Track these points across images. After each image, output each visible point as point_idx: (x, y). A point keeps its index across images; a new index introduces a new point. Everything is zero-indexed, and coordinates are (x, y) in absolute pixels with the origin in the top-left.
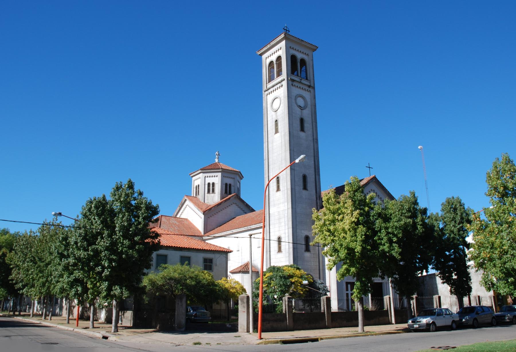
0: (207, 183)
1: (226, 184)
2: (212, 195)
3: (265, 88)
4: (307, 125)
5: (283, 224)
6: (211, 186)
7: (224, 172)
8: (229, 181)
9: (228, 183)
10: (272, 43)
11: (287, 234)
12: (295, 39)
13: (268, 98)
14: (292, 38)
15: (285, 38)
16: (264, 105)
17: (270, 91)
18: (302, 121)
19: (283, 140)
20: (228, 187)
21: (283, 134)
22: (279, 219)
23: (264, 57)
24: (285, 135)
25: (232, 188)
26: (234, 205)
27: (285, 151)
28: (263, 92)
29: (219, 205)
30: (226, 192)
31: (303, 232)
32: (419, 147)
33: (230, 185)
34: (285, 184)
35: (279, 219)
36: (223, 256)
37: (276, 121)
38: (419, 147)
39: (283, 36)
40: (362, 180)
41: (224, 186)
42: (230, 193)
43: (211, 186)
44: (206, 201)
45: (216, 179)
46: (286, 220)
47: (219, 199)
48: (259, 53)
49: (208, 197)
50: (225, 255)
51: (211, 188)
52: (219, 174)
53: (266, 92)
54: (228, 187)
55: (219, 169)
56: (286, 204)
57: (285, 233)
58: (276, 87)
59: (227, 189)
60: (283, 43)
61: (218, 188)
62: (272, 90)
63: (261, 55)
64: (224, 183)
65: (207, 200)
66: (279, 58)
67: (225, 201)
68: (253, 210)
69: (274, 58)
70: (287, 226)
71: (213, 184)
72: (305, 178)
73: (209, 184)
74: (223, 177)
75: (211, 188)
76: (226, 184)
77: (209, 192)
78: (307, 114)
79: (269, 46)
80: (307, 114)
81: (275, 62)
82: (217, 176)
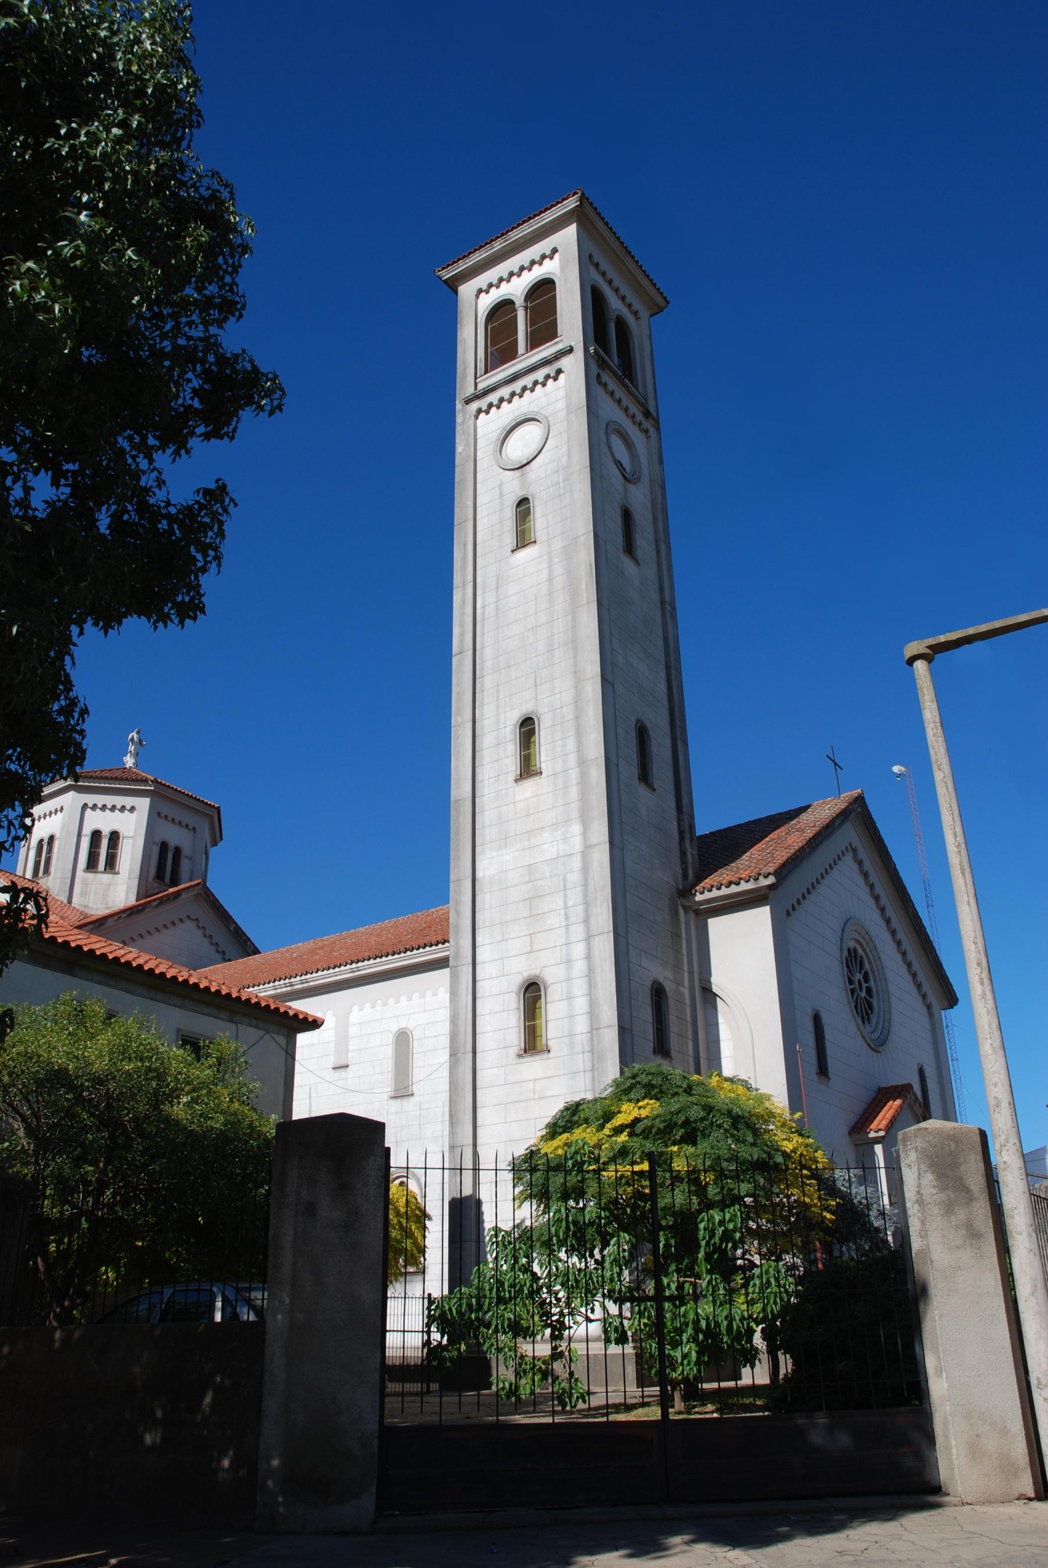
0: (87, 831)
1: (164, 846)
2: (106, 877)
3: (466, 387)
4: (644, 541)
5: (556, 920)
6: (105, 843)
7: (167, 800)
8: (175, 836)
9: (173, 843)
10: (515, 235)
11: (580, 966)
12: (607, 234)
13: (481, 430)
14: (600, 225)
15: (578, 215)
16: (459, 449)
17: (494, 398)
18: (627, 516)
19: (559, 570)
20: (170, 856)
21: (557, 545)
22: (533, 899)
23: (467, 290)
24: (568, 550)
25: (185, 865)
26: (190, 926)
27: (573, 609)
28: (459, 406)
29: (130, 912)
30: (160, 875)
31: (645, 962)
32: (896, 769)
33: (178, 851)
34: (571, 744)
35: (533, 899)
36: (272, 1042)
37: (523, 504)
38: (896, 769)
39: (571, 203)
40: (804, 809)
41: (156, 851)
42: (175, 882)
43: (105, 843)
44: (76, 900)
45: (130, 821)
46: (575, 897)
47: (137, 900)
48: (446, 274)
49: (85, 883)
50: (282, 1041)
51: (102, 851)
52: (143, 804)
53: (475, 406)
54: (170, 856)
55: (144, 781)
56: (576, 829)
57: (568, 962)
58: (527, 381)
59: (164, 865)
60: (571, 231)
61: (131, 855)
62: (505, 392)
63: (453, 285)
64: (158, 840)
65: (83, 894)
66: (544, 288)
67: (162, 901)
68: (256, 951)
69: (517, 289)
70: (578, 932)
71: (114, 837)
72: (642, 733)
73: (96, 835)
74: (155, 815)
75: (102, 851)
76: (164, 846)
77: (92, 864)
78: (639, 497)
79: (498, 246)
80: (639, 497)
81: (519, 302)
82: (132, 809)
